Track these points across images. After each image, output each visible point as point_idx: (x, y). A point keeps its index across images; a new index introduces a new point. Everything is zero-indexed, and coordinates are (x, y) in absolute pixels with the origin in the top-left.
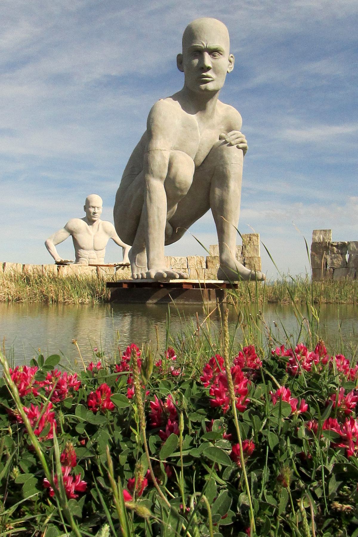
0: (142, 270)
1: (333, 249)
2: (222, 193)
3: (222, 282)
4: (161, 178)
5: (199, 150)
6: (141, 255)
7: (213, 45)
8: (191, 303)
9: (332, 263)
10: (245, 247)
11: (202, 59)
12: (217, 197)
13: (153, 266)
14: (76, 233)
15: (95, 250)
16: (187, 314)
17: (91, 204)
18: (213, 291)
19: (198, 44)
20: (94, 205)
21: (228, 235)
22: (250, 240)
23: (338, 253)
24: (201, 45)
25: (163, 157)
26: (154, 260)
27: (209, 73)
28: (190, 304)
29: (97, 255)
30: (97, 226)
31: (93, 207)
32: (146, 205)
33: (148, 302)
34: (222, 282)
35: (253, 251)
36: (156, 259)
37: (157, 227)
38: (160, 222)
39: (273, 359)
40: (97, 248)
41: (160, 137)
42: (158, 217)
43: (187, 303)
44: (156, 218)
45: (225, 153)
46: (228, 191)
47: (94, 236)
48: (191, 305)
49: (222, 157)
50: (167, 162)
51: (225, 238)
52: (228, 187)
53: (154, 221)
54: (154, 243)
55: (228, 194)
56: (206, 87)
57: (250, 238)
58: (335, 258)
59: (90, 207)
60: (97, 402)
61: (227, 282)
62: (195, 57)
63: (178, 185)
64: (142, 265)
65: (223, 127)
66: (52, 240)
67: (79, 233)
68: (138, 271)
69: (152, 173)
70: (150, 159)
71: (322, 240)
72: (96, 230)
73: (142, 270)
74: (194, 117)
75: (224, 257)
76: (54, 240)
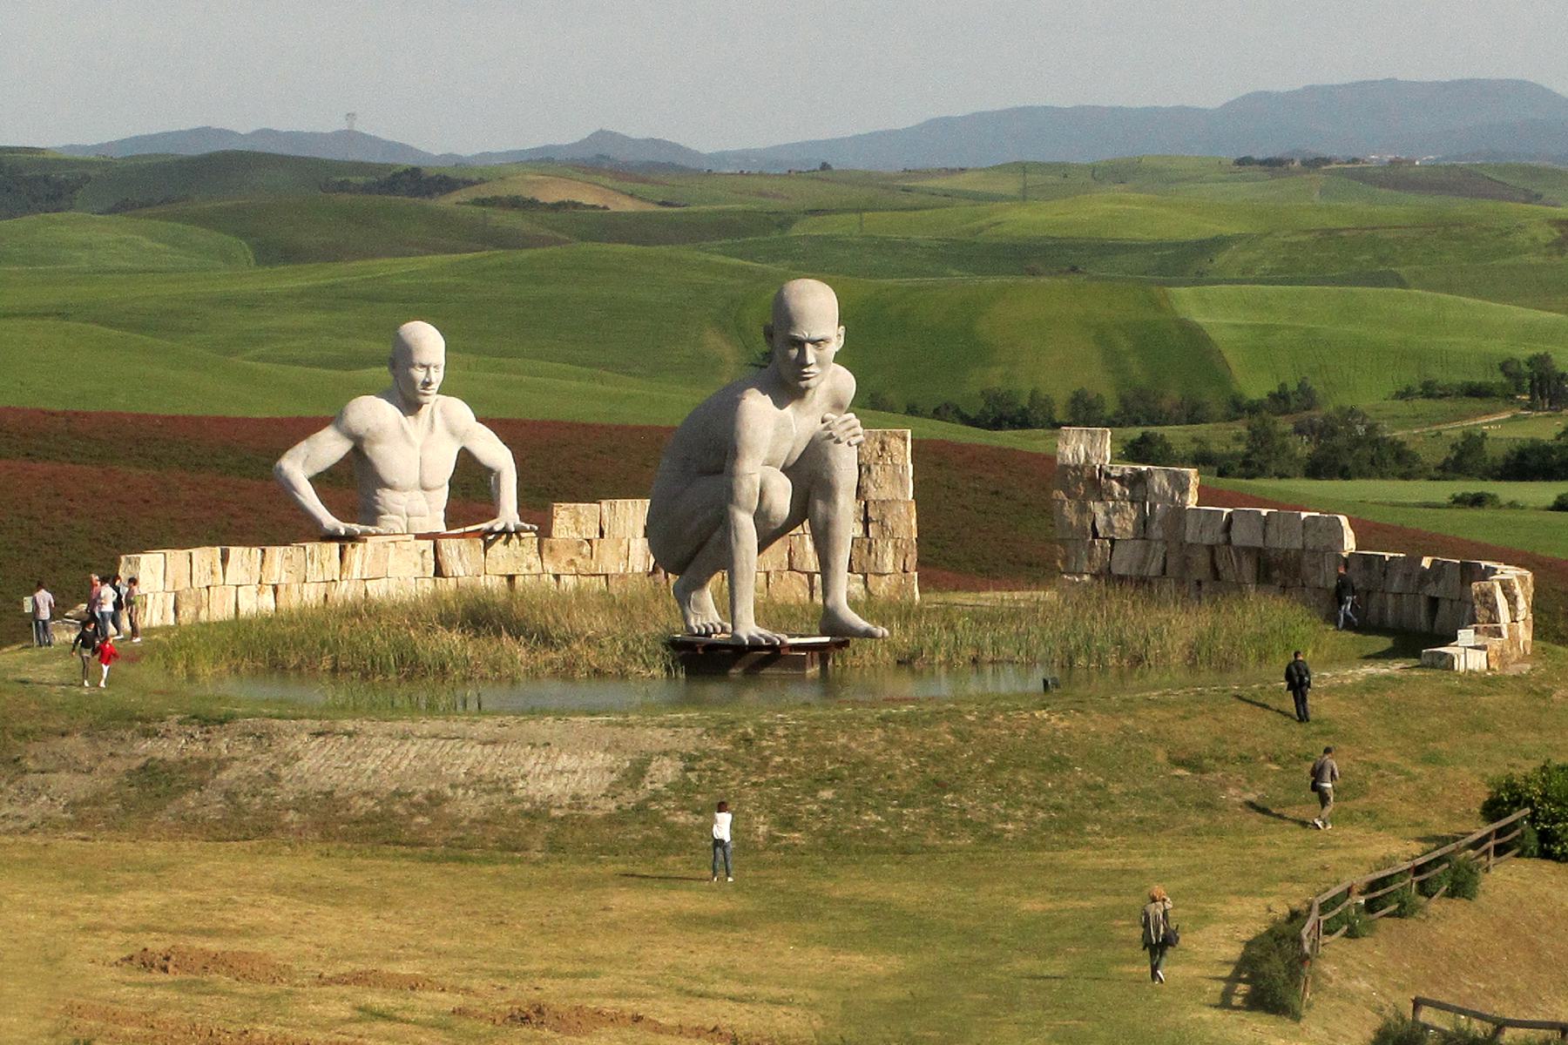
1: (1111, 487)
3: (827, 639)
4: (749, 511)
7: (816, 335)
9: (1110, 525)
10: (869, 469)
11: (803, 353)
14: (373, 442)
15: (424, 488)
17: (418, 358)
18: (816, 655)
20: (425, 362)
22: (883, 449)
23: (1123, 494)
25: (753, 484)
27: (811, 369)
29: (429, 503)
34: (827, 639)
35: (892, 483)
40: (429, 483)
45: (831, 454)
47: (422, 448)
51: (831, 573)
52: (835, 502)
57: (882, 443)
58: (1115, 511)
59: (413, 365)
60: (1106, 575)
67: (379, 441)
69: (738, 504)
70: (736, 487)
71: (1082, 459)
72: (426, 428)
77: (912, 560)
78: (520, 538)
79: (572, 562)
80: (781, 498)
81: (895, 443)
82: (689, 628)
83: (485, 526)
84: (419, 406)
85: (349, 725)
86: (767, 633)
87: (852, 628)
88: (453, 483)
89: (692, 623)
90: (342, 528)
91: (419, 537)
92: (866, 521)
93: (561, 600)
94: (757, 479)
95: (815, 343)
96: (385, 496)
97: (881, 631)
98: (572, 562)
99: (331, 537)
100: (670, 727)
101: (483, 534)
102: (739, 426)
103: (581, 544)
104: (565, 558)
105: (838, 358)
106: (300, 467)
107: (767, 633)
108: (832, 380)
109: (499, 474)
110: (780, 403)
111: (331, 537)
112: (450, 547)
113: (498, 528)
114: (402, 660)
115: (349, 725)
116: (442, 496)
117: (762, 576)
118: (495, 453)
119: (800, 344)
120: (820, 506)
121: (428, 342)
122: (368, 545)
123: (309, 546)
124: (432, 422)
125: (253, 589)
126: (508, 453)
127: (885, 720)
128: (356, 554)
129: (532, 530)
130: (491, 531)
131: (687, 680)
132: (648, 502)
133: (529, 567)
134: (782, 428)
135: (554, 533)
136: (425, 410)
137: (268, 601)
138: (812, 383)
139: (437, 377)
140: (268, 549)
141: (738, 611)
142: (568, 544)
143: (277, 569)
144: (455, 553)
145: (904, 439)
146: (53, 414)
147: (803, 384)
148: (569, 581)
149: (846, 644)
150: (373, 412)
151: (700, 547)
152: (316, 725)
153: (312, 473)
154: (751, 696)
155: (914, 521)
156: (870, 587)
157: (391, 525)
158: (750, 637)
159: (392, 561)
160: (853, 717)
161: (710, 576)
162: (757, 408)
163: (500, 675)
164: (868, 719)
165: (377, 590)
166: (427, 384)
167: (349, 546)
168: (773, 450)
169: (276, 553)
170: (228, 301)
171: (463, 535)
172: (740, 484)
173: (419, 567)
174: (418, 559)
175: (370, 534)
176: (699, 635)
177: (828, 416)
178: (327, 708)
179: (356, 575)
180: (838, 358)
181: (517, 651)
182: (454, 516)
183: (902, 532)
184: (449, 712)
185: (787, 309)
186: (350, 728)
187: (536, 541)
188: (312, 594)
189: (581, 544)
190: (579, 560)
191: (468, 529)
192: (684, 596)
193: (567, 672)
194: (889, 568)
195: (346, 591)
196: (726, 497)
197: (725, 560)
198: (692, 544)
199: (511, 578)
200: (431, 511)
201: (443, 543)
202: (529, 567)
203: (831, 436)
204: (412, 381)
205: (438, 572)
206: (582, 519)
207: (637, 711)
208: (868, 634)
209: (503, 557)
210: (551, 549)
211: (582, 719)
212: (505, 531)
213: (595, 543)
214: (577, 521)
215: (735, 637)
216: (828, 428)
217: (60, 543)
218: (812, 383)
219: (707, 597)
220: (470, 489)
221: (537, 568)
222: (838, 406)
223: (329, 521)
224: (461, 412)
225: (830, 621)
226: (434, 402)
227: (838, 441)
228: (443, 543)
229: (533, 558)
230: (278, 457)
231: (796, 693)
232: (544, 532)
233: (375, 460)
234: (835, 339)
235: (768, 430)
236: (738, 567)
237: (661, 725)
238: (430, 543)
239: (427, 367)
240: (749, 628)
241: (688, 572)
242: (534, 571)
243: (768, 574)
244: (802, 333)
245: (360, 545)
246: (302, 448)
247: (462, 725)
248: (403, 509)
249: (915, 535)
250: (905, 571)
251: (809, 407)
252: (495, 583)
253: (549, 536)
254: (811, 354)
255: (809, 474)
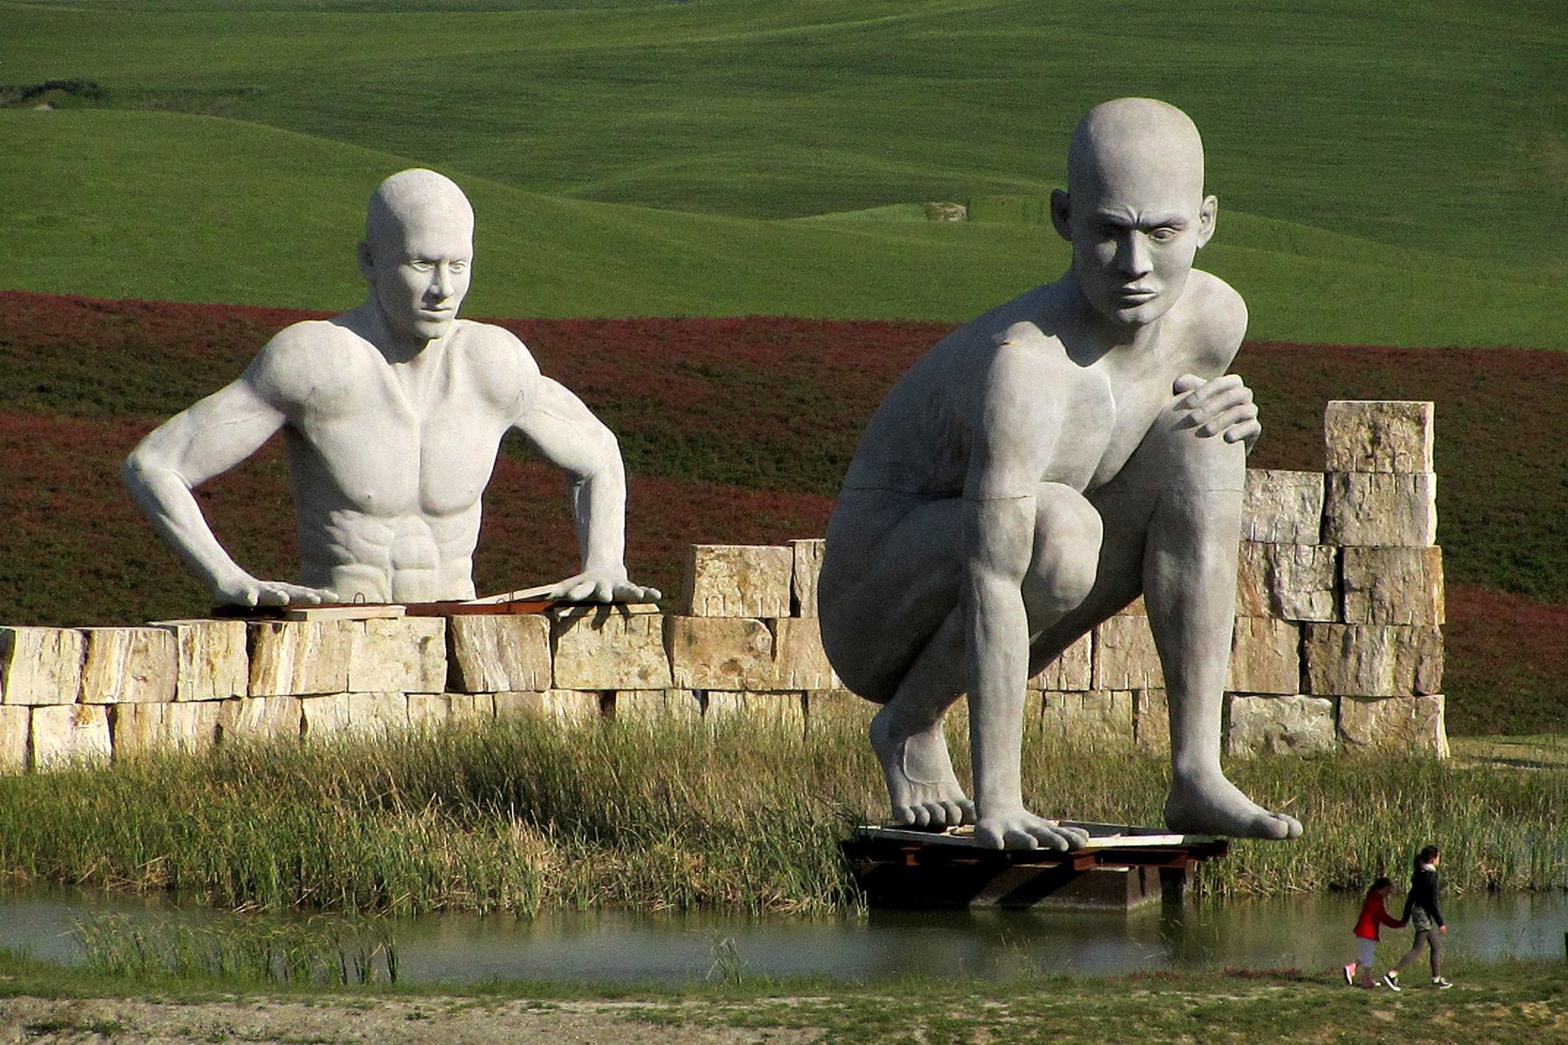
0: (925, 793)
2: (1181, 575)
3: (1176, 839)
5: (1112, 444)
6: (921, 744)
7: (1155, 214)
8: (1094, 907)
10: (1346, 482)
11: (1126, 251)
12: (1165, 585)
13: (993, 810)
14: (321, 415)
15: (429, 510)
16: (1082, 934)
17: (415, 245)
18: (1153, 872)
19: (1115, 212)
20: (432, 251)
21: (1199, 697)
22: (1375, 441)
24: (1126, 217)
25: (1021, 519)
26: (994, 792)
27: (1144, 284)
28: (1091, 909)
29: (439, 540)
30: (438, 364)
31: (426, 261)
32: (974, 648)
33: (973, 903)
34: (1176, 839)
35: (1394, 512)
36: (1001, 790)
37: (1004, 705)
38: (1010, 691)
39: (541, 781)
40: (440, 499)
41: (1012, 462)
42: (1008, 680)
43: (1082, 906)
44: (1001, 685)
45: (1189, 458)
46: (1199, 572)
47: (425, 428)
48: (1093, 912)
49: (1180, 469)
50: (1031, 530)
51: (1189, 703)
52: (1197, 557)
53: (995, 690)
54: (994, 747)
55: (1197, 580)
56: (1137, 316)
57: (1374, 428)
59: (406, 259)
61: (1192, 839)
62: (1107, 236)
63: (1059, 593)
64: (926, 777)
65: (1183, 356)
66: (175, 455)
67: (337, 415)
68: (913, 796)
69: (990, 561)
70: (985, 524)
73: (925, 793)
74: (1101, 369)
75: (1185, 764)
76: (185, 457)
77: (1433, 668)
78: (627, 616)
79: (733, 665)
80: (1080, 546)
81: (1401, 430)
82: (898, 812)
83: (555, 590)
84: (421, 342)
85: (108, 1011)
86: (1048, 826)
87: (1225, 816)
88: (492, 498)
89: (906, 805)
90: (253, 589)
91: (415, 610)
92: (1339, 590)
93: (679, 748)
94: (1029, 509)
95: (1155, 230)
96: (350, 525)
97: (1288, 823)
98: (733, 665)
99: (232, 609)
100: (752, 1027)
101: (550, 607)
102: (994, 400)
103: (752, 629)
104: (719, 658)
105: (1203, 260)
106: (181, 460)
107: (1048, 826)
108: (1193, 306)
109: (589, 482)
110: (1081, 353)
111: (232, 609)
112: (478, 633)
113: (579, 593)
114: (293, 872)
115: (108, 1011)
116: (467, 527)
117: (1124, 699)
118: (582, 439)
119: (1122, 232)
120: (1166, 565)
121: (441, 212)
122: (308, 626)
123: (185, 627)
124: (447, 375)
125: (65, 712)
126: (608, 439)
127: (1202, 1016)
128: (282, 645)
129: (648, 599)
130: (564, 601)
131: (873, 920)
132: (807, 557)
133: (644, 675)
134: (1085, 405)
135: (698, 606)
136: (432, 354)
137: (96, 734)
138: (1147, 312)
139: (456, 283)
140: (98, 633)
141: (988, 781)
142: (726, 629)
143: (115, 672)
144: (490, 646)
145: (1420, 421)
146: (98, 308)
147: (1127, 314)
148: (724, 704)
149: (1220, 849)
150: (324, 353)
151: (920, 647)
152: (42, 1009)
153: (198, 477)
154: (1016, 962)
155: (1437, 592)
156: (1346, 725)
157: (360, 586)
158: (1010, 836)
159: (357, 662)
160: (1139, 1011)
161: (942, 706)
162: (1034, 364)
163: (493, 912)
164: (1171, 1014)
165: (323, 718)
166: (434, 299)
167: (268, 626)
168: (1066, 448)
169: (115, 641)
170: (576, 69)
171: (508, 609)
172: (994, 520)
173: (416, 672)
174: (412, 654)
175: (310, 604)
176: (918, 826)
177: (1188, 379)
178: (82, 974)
179: (282, 686)
180: (1203, 260)
181: (534, 853)
182: (498, 563)
183: (1412, 613)
184: (334, 981)
185: (391, 213)
186: (110, 1017)
187: (658, 622)
188: (188, 727)
189: (752, 629)
190: (747, 662)
191: (519, 595)
192: (890, 745)
193: (628, 902)
194: (1385, 686)
195: (260, 720)
196: (968, 546)
197: (962, 676)
198: (905, 647)
199: (607, 698)
200: (445, 560)
201: (466, 624)
202: (644, 675)
203: (1190, 422)
204: (404, 292)
205: (456, 682)
206: (754, 578)
207: (704, 990)
208: (1259, 831)
209: (589, 653)
210: (691, 639)
211: (580, 1006)
212: (594, 600)
213: (781, 628)
214: (743, 583)
215: (983, 834)
216: (1184, 405)
217: (21, 578)
218: (1147, 312)
219: (937, 749)
220: (527, 513)
221: (660, 678)
222: (1208, 360)
223: (229, 574)
224: (509, 355)
225: (1188, 807)
226: (451, 334)
227: (1204, 433)
228: (466, 624)
229: (652, 657)
230: (137, 434)
231: (1106, 959)
232: (677, 601)
233: (330, 454)
234: (1195, 223)
235: (1055, 410)
236: (987, 689)
237: (739, 1022)
238: (433, 627)
239: (436, 263)
240: (1010, 815)
241: (903, 693)
242: (654, 681)
243: (1136, 694)
244: (1125, 210)
245: (292, 626)
246: (180, 425)
247: (335, 1014)
248: (386, 553)
249: (1439, 619)
250: (1417, 693)
251: (1147, 360)
252: (566, 707)
253: (687, 611)
254: (1143, 253)
255: (1144, 505)
